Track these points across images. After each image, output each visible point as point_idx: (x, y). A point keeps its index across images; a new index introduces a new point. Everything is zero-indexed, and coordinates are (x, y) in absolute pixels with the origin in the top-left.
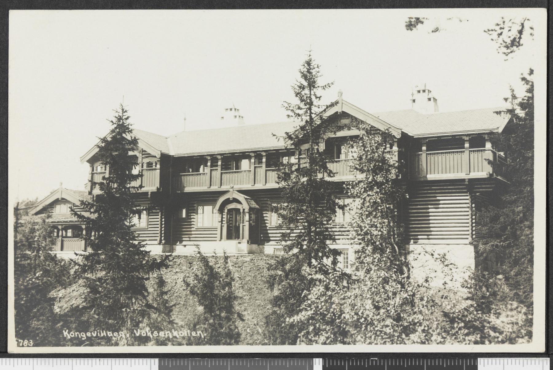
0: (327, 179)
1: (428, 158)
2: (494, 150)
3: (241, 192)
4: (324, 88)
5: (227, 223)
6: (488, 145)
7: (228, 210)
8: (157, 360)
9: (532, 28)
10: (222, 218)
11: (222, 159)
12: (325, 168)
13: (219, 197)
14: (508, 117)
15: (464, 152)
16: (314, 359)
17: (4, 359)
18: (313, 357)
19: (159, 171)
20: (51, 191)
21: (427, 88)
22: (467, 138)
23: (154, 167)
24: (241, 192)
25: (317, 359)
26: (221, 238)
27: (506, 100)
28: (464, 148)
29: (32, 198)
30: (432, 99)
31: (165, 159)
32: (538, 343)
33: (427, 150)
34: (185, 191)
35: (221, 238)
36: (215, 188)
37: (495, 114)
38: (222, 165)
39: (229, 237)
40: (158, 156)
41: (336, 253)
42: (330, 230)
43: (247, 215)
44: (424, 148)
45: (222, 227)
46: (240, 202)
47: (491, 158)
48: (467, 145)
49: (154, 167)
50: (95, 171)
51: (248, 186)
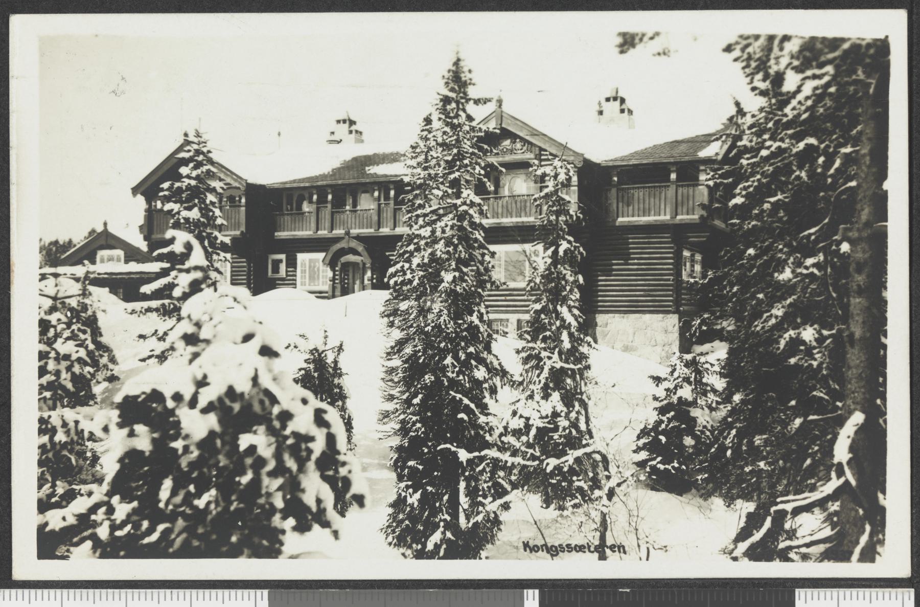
1: (620, 194)
5: (341, 282)
7: (342, 264)
8: (266, 592)
9: (248, 338)
10: (334, 275)
13: (330, 246)
15: (668, 186)
16: (525, 591)
17: (7, 591)
18: (524, 588)
19: (243, 209)
21: (620, 94)
25: (531, 591)
30: (626, 111)
31: (255, 192)
32: (895, 557)
37: (252, 374)
40: (243, 188)
49: (237, 203)
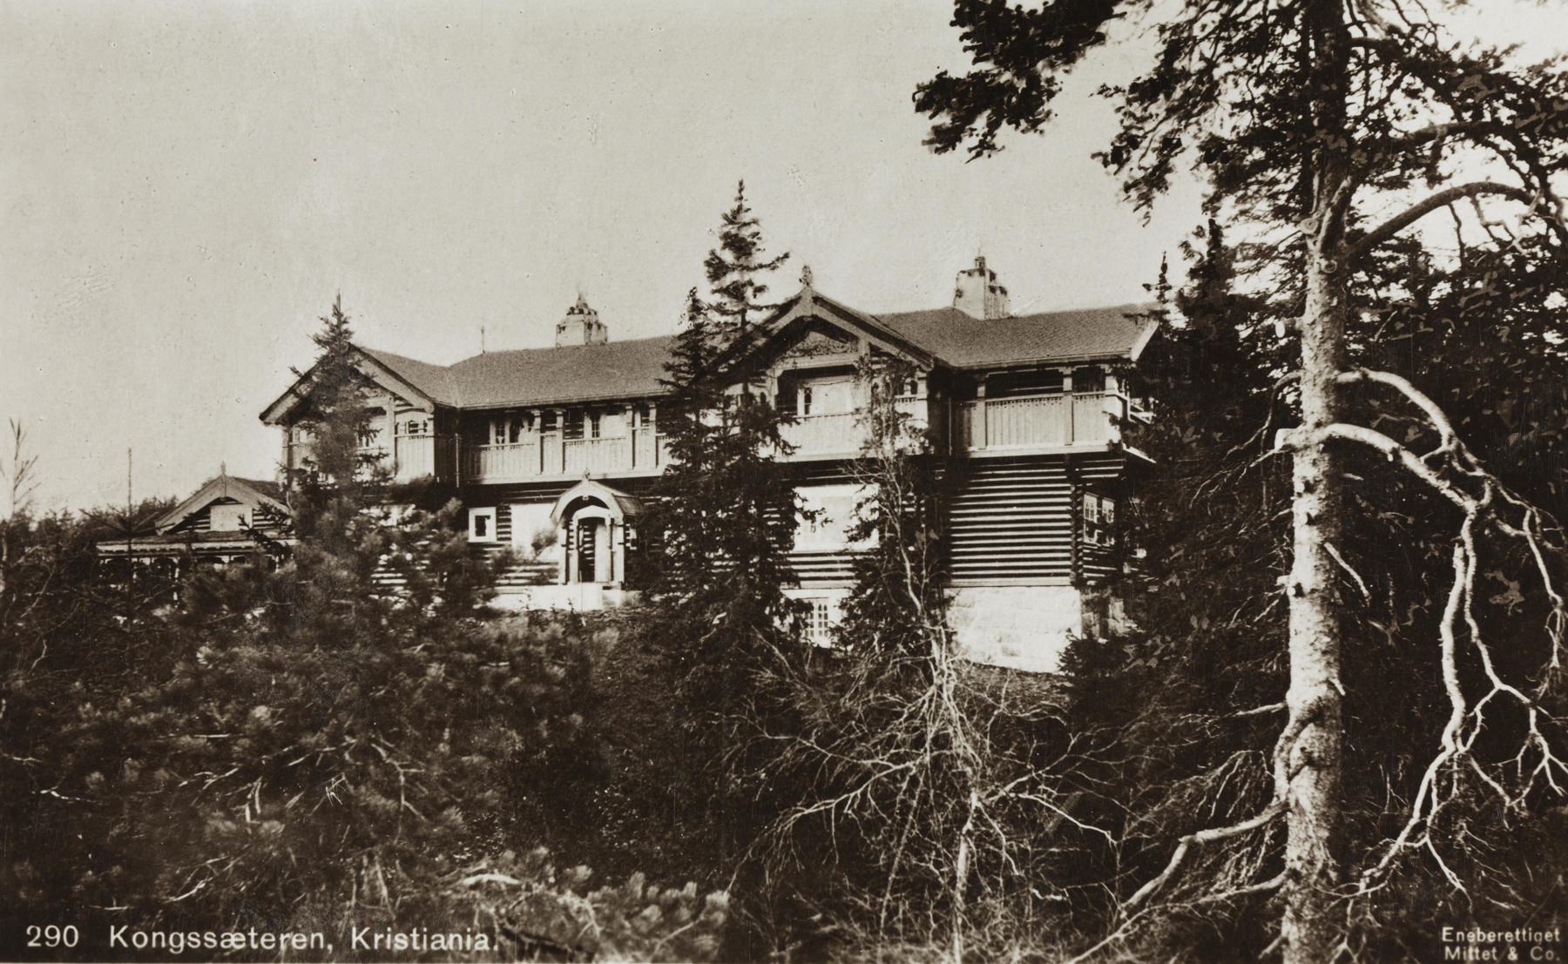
0: (780, 458)
2: (1122, 395)
3: (605, 482)
4: (772, 266)
6: (1111, 383)
10: (569, 537)
11: (1073, 375)
12: (775, 437)
14: (1152, 327)
20: (205, 480)
22: (1068, 371)
23: (421, 433)
24: (605, 482)
26: (567, 579)
27: (1148, 287)
28: (1061, 390)
29: (163, 497)
33: (988, 395)
34: (487, 482)
35: (567, 579)
36: (552, 474)
38: (565, 427)
39: (584, 580)
41: (803, 607)
42: (1243, 19)
43: (620, 530)
44: (981, 390)
45: (568, 557)
46: (602, 504)
47: (1119, 414)
48: (1068, 383)
50: (295, 441)
51: (622, 471)
